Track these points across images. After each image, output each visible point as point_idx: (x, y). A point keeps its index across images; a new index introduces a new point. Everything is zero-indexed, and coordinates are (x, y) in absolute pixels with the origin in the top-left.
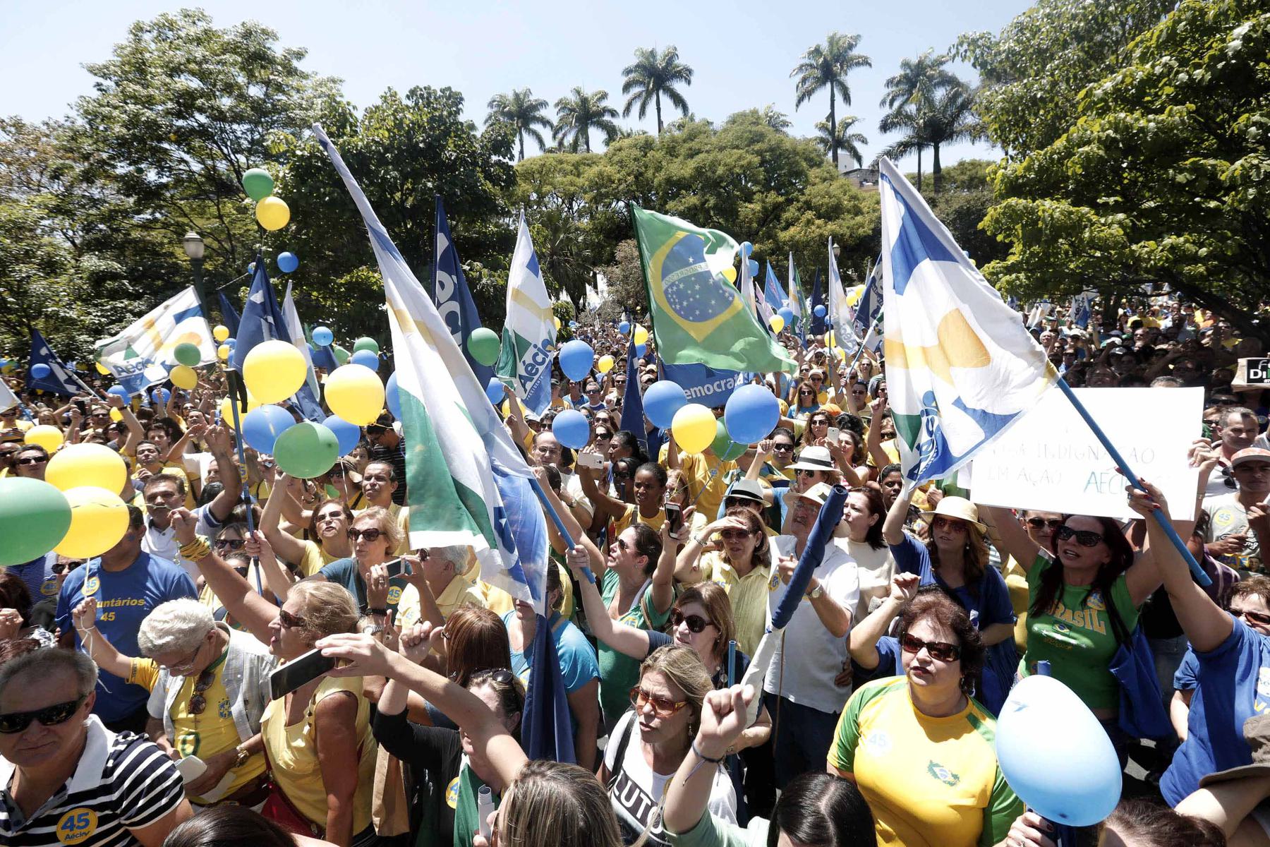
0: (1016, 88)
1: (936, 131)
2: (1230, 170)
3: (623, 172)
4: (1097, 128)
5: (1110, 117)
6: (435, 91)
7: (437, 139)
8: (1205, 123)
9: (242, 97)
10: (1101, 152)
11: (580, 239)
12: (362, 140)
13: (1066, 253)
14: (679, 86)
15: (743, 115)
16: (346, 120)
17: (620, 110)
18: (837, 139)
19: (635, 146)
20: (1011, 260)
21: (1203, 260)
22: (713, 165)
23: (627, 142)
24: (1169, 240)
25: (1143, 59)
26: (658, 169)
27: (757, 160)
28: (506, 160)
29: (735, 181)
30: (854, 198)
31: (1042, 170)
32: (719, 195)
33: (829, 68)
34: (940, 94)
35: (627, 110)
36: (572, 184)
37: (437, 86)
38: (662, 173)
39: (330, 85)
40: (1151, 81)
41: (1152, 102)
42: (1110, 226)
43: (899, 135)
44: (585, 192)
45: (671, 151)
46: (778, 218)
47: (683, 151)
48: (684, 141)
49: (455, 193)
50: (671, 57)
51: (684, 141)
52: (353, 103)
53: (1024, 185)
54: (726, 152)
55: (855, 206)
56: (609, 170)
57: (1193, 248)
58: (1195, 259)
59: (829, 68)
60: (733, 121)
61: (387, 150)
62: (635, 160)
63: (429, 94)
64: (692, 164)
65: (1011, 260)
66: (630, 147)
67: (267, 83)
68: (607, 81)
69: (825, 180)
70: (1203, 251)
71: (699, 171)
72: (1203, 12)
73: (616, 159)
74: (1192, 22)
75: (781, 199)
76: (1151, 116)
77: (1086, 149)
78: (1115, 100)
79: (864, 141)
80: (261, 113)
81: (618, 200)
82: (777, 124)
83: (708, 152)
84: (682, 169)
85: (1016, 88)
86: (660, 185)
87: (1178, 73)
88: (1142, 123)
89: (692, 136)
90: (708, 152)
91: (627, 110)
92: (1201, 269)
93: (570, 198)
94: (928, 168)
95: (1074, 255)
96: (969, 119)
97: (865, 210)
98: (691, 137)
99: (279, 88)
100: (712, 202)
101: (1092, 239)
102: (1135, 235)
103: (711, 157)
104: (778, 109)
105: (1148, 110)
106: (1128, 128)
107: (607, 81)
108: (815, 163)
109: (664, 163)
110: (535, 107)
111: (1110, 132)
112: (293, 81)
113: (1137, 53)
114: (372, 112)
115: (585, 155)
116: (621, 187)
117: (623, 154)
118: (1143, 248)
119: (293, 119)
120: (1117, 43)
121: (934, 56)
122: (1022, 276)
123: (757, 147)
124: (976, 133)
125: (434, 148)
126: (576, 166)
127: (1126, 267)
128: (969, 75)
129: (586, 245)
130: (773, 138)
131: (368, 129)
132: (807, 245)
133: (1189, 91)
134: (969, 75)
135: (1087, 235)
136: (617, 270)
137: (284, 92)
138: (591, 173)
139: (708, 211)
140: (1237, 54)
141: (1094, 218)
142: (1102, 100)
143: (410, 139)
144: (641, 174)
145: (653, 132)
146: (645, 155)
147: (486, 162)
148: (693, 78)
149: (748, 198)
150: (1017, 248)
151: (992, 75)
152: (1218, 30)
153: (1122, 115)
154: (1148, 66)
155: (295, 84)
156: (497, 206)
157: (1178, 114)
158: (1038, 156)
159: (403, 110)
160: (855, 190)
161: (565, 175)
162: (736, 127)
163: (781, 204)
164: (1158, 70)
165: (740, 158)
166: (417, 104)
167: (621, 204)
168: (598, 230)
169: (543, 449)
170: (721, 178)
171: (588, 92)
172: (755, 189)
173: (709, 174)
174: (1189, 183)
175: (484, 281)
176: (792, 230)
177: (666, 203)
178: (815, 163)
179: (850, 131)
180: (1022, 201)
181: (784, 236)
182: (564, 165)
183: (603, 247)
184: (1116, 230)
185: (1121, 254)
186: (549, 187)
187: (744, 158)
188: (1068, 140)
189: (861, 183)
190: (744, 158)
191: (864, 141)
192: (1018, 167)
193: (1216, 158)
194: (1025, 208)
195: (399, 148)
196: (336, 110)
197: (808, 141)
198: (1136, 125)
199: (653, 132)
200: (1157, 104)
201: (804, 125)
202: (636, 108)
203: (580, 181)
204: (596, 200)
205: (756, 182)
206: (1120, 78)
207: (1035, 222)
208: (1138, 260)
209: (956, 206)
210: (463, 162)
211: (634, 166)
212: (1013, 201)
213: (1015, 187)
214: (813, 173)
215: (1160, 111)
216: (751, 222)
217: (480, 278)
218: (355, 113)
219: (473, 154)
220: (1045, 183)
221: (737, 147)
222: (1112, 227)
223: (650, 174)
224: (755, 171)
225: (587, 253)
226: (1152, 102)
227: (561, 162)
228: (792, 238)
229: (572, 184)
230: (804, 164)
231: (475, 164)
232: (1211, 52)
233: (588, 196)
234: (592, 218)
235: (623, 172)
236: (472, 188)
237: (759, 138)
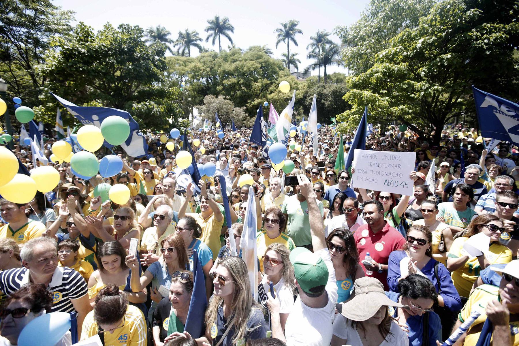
0: (355, 49)
1: (326, 61)
2: (418, 85)
3: (205, 66)
4: (380, 68)
5: (384, 64)
6: (131, 27)
7: (133, 47)
8: (411, 69)
9: (21, 15)
10: (381, 76)
11: (187, 93)
12: (97, 44)
13: (370, 109)
14: (229, 32)
15: (255, 47)
16: (89, 34)
17: (204, 39)
18: (291, 61)
19: (210, 56)
20: (353, 111)
21: (411, 114)
22: (242, 66)
23: (206, 54)
24: (401, 107)
25: (394, 46)
26: (220, 66)
27: (259, 66)
28: (162, 59)
29: (251, 74)
30: (296, 83)
31: (364, 80)
32: (244, 79)
33: (289, 32)
34: (327, 46)
35: (207, 39)
36: (183, 70)
37: (132, 25)
38: (222, 68)
39: (70, 14)
40: (396, 54)
41: (396, 60)
42: (384, 101)
43: (313, 61)
44: (189, 74)
45: (225, 59)
46: (267, 89)
47: (230, 60)
48: (231, 56)
49: (141, 71)
50: (225, 21)
51: (231, 56)
52: (92, 27)
53: (358, 84)
54: (247, 62)
55: (296, 87)
56: (199, 65)
57: (407, 109)
58: (408, 113)
59: (289, 32)
60: (250, 49)
61: (109, 49)
62: (210, 62)
63: (129, 28)
64: (234, 65)
65: (353, 111)
66: (208, 56)
67: (36, 10)
68: (200, 28)
69: (285, 76)
70: (411, 111)
71: (236, 69)
72: (411, 34)
73: (202, 60)
74: (408, 36)
75: (269, 82)
76: (396, 66)
77: (377, 74)
78: (386, 59)
79: (300, 62)
80: (32, 23)
81: (203, 78)
82: (268, 52)
83: (240, 61)
84: (230, 67)
85: (355, 49)
86: (220, 73)
87: (404, 52)
88: (394, 67)
89: (233, 55)
90: (240, 61)
91: (207, 39)
92: (410, 117)
93: (182, 75)
94: (322, 74)
95: (373, 110)
96: (336, 57)
97: (300, 88)
98: (233, 54)
99: (43, 13)
100: (242, 81)
101: (379, 105)
102: (392, 104)
103: (241, 63)
104: (268, 47)
105: (395, 63)
106: (389, 69)
107: (200, 28)
108: (282, 69)
109: (222, 64)
110: (165, 35)
111: (384, 69)
112: (49, 10)
113: (392, 44)
114: (102, 33)
115: (188, 57)
116: (204, 73)
117: (204, 59)
118: (394, 109)
119: (51, 29)
120: (386, 36)
121: (325, 32)
122: (357, 116)
123: (259, 61)
124: (339, 63)
125: (131, 51)
126: (185, 62)
127: (389, 115)
128: (337, 41)
129: (189, 96)
130: (266, 57)
131: (100, 39)
132: (278, 100)
133: (406, 59)
134: (337, 41)
135: (377, 103)
136: (204, 107)
137: (45, 15)
138: (192, 65)
139: (240, 85)
140: (420, 48)
141: (380, 98)
142: (382, 58)
143: (121, 47)
144: (213, 68)
145: (217, 51)
146: (214, 60)
147: (153, 59)
148: (234, 31)
149: (256, 80)
150: (355, 106)
151: (347, 42)
152: (415, 40)
153: (387, 64)
154: (395, 49)
155: (50, 12)
156: (159, 78)
157: (404, 66)
158: (362, 75)
159: (117, 33)
160: (296, 80)
161: (180, 66)
162: (252, 52)
163: (268, 84)
164: (398, 50)
165: (253, 64)
166: (123, 31)
167: (204, 80)
168: (194, 90)
169: (165, 186)
170: (246, 72)
171: (190, 31)
172: (259, 77)
173: (241, 70)
174: (407, 88)
175: (155, 110)
176: (273, 94)
177: (223, 80)
178: (282, 69)
179: (295, 57)
180: (357, 91)
181: (270, 96)
182: (179, 62)
183: (196, 97)
184: (386, 103)
185: (387, 110)
186: (173, 70)
187: (255, 65)
188: (372, 71)
189: (298, 78)
190: (255, 65)
191: (300, 62)
192: (356, 79)
193: (414, 81)
194: (359, 93)
195: (115, 50)
196: (84, 29)
197: (278, 60)
198: (392, 68)
199: (217, 51)
200: (398, 62)
201: (277, 55)
202: (211, 39)
203: (186, 69)
204: (194, 77)
205: (259, 75)
206: (387, 52)
207: (361, 98)
208: (392, 113)
209: (332, 89)
210: (144, 59)
211: (209, 64)
212: (355, 90)
213: (355, 86)
214: (281, 73)
215: (399, 64)
216: (257, 90)
217: (154, 108)
218: (93, 31)
219: (147, 55)
220: (364, 85)
221: (252, 60)
222: (384, 101)
223: (216, 68)
224: (259, 70)
225: (190, 99)
226: (396, 60)
227: (178, 60)
228: (273, 98)
229: (183, 70)
230: (277, 69)
231: (149, 59)
232: (413, 47)
233: (190, 75)
234: (191, 84)
235: (205, 66)
236: (148, 70)
237: (260, 57)
